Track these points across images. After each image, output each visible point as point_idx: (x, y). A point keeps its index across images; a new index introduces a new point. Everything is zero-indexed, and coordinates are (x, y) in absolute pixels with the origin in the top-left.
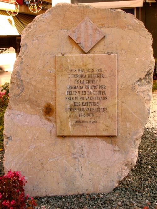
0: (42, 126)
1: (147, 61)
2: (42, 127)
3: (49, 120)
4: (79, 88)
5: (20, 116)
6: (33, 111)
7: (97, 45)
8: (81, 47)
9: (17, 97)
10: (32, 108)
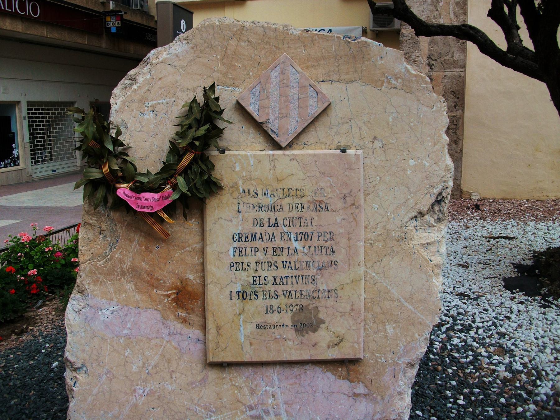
0: (167, 338)
1: (437, 168)
2: (167, 342)
3: (184, 321)
4: (264, 238)
5: (108, 312)
6: (142, 301)
7: (312, 128)
8: (270, 133)
9: (101, 263)
10: (139, 290)
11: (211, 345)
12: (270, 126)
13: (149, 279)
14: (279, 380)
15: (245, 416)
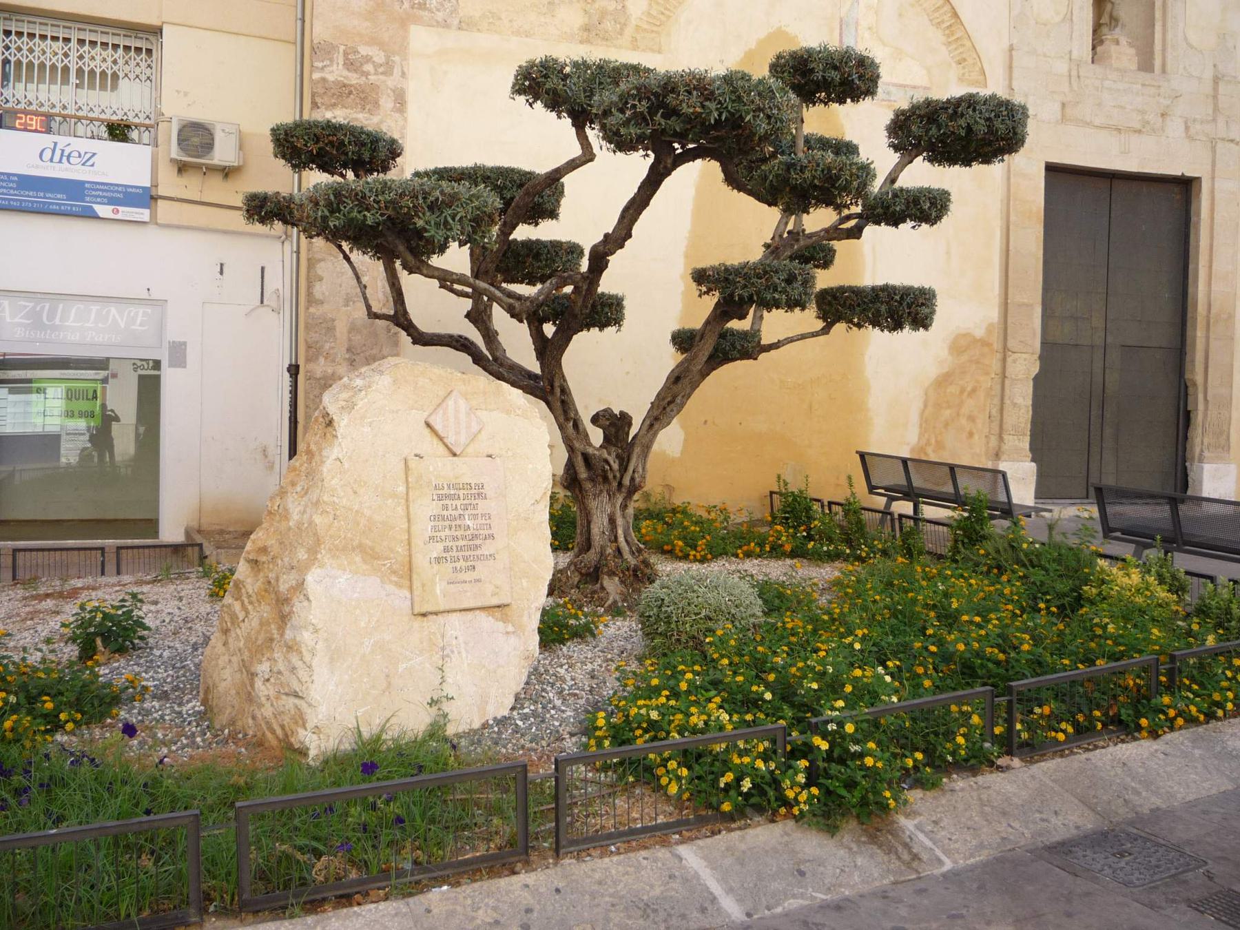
10: (365, 561)
11: (416, 599)
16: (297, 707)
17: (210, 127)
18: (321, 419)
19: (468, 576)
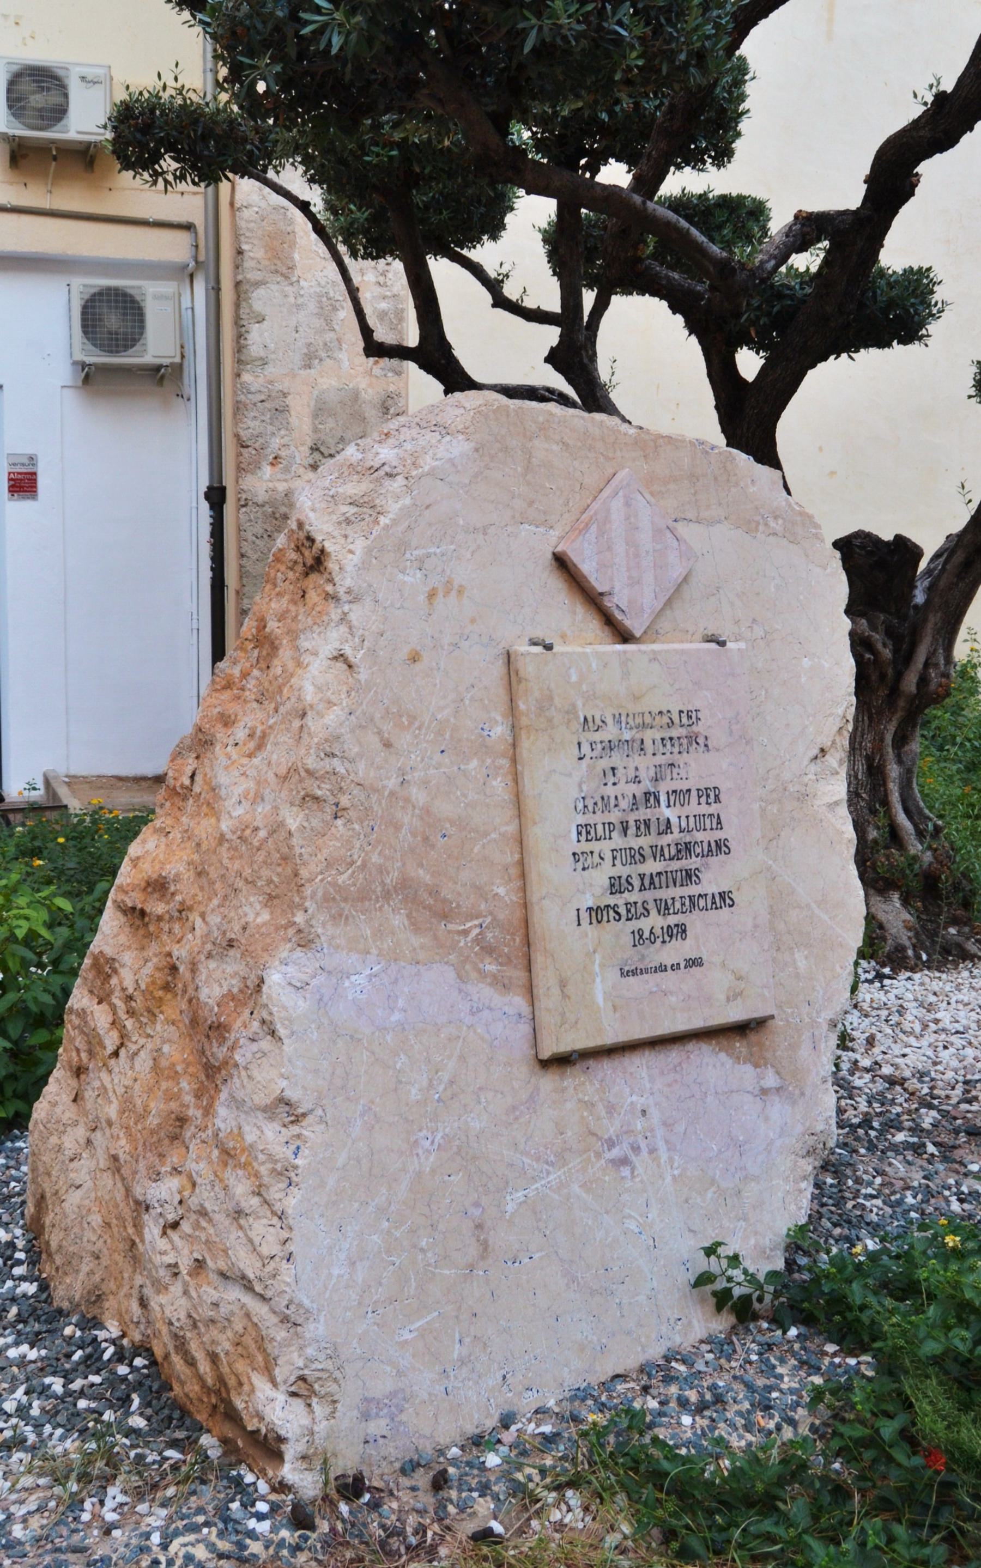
0: (468, 1020)
2: (469, 1027)
5: (360, 980)
10: (416, 928)
12: (615, 600)
13: (432, 902)
14: (652, 1080)
15: (603, 1161)
16: (248, 1315)
17: (61, 73)
18: (293, 556)
19: (673, 952)
